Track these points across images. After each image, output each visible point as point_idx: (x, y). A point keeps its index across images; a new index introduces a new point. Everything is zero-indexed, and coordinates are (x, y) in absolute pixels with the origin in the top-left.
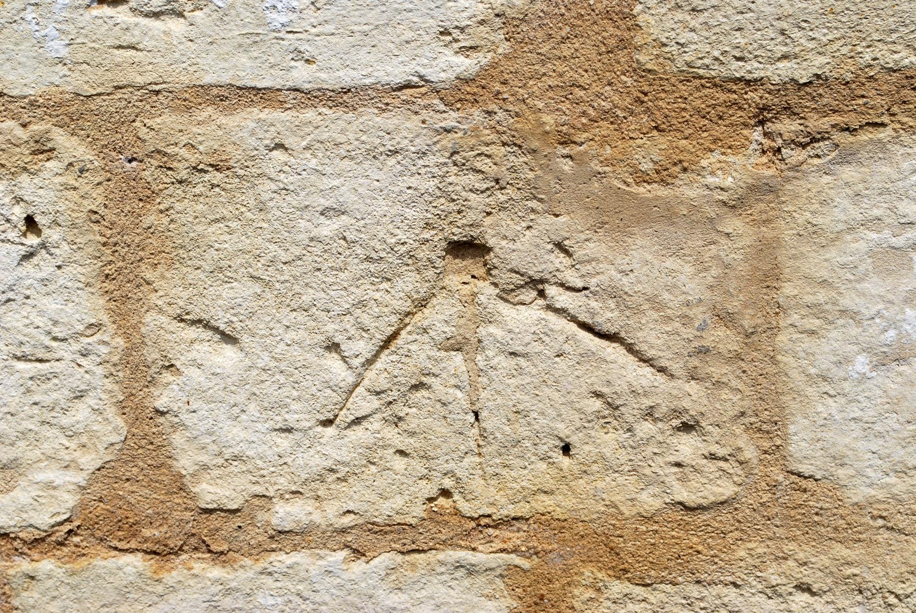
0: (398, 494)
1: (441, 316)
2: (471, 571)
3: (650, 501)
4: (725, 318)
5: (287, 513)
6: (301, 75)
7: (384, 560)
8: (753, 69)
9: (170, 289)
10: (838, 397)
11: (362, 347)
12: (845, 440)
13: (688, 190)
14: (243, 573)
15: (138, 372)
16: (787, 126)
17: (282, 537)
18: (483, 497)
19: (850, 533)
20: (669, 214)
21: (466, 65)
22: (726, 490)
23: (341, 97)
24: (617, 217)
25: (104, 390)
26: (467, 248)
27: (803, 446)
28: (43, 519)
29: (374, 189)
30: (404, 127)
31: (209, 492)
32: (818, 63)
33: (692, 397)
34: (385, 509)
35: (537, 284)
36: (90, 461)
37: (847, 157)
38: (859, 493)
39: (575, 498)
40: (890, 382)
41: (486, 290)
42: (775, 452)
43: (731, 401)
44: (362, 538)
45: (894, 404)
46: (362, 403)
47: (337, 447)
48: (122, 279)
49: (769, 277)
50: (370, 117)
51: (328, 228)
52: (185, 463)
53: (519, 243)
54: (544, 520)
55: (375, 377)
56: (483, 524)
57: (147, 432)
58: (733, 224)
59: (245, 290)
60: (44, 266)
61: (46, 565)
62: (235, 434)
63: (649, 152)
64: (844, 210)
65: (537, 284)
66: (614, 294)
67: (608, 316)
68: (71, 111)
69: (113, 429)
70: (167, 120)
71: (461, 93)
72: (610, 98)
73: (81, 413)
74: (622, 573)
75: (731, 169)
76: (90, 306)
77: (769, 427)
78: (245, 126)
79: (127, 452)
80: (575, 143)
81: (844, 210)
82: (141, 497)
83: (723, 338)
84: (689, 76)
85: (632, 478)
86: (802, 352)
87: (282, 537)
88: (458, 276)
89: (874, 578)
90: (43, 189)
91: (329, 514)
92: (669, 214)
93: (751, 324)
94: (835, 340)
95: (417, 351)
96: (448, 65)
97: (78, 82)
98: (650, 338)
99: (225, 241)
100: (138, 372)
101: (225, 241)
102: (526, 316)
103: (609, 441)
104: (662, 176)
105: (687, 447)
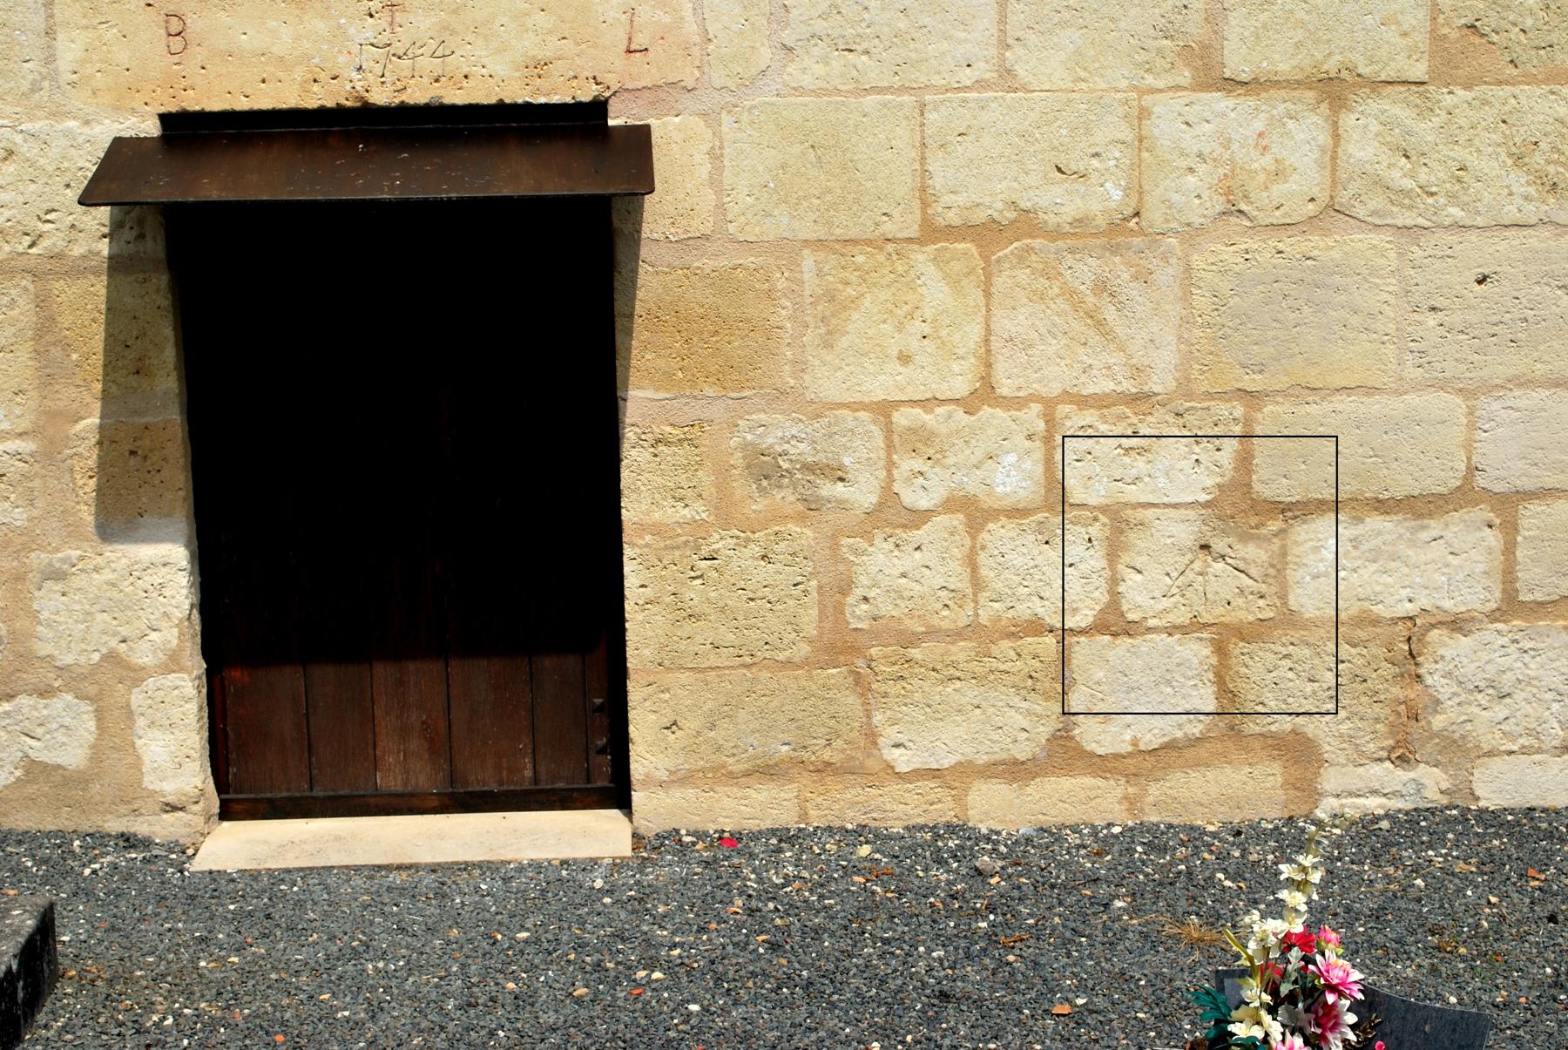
0: (1182, 617)
1: (1197, 566)
2: (1201, 639)
3: (1251, 618)
4: (1272, 566)
5: (1152, 623)
6: (1166, 500)
7: (1177, 636)
8: (1281, 499)
9: (1126, 558)
10: (1540, 227)
11: (1175, 574)
12: (1304, 600)
13: (1264, 531)
14: (1138, 641)
15: (1114, 581)
16: (1289, 514)
17: (1149, 630)
18: (1206, 618)
19: (1304, 627)
20: (1258, 537)
21: (1209, 497)
22: (1272, 615)
23: (1175, 506)
24: (1245, 538)
25: (1104, 586)
26: (1205, 547)
27: (1293, 603)
28: (1083, 625)
29: (1182, 531)
30: (1191, 514)
31: (1131, 616)
32: (1298, 497)
33: (1263, 588)
34: (1179, 621)
35: (1223, 557)
36: (1098, 608)
37: (1304, 522)
38: (1307, 616)
39: (1232, 617)
40: (1315, 584)
41: (1209, 559)
42: (1285, 604)
43: (1274, 589)
44: (1170, 630)
45: (1317, 590)
46: (1174, 590)
47: (1167, 603)
48: (1112, 557)
49: (1284, 555)
50: (1183, 511)
51: (1169, 541)
52: (1124, 608)
53: (1219, 545)
54: (1222, 624)
55: (1179, 583)
56: (1206, 625)
57: (1115, 597)
58: (1275, 540)
59: (1145, 558)
60: (1092, 551)
61: (1083, 639)
62: (1139, 599)
63: (1253, 521)
64: (1303, 536)
65: (1223, 557)
66: (1244, 559)
67: (1241, 566)
68: (1104, 509)
69: (1105, 598)
70: (1129, 512)
71: (1206, 505)
72: (1244, 506)
73: (1097, 594)
74: (1243, 640)
75: (1274, 525)
76: (1104, 563)
77: (1283, 597)
78: (1150, 513)
79: (1108, 606)
80: (720, 207)
81: (1303, 536)
82: (1111, 618)
83: (1272, 571)
84: (1265, 501)
85: (1247, 612)
86: (1293, 575)
87: (1149, 630)
88: (1202, 555)
89: (1311, 640)
90: (1094, 531)
91: (1163, 623)
92: (1258, 537)
93: (1279, 569)
94: (1301, 572)
95: (1190, 575)
96: (1203, 497)
97: (1107, 501)
98: (1253, 571)
99: (1141, 544)
100: (1114, 581)
101: (1141, 544)
102: (1220, 565)
103: (1240, 601)
104: (1257, 527)
105: (1261, 602)
